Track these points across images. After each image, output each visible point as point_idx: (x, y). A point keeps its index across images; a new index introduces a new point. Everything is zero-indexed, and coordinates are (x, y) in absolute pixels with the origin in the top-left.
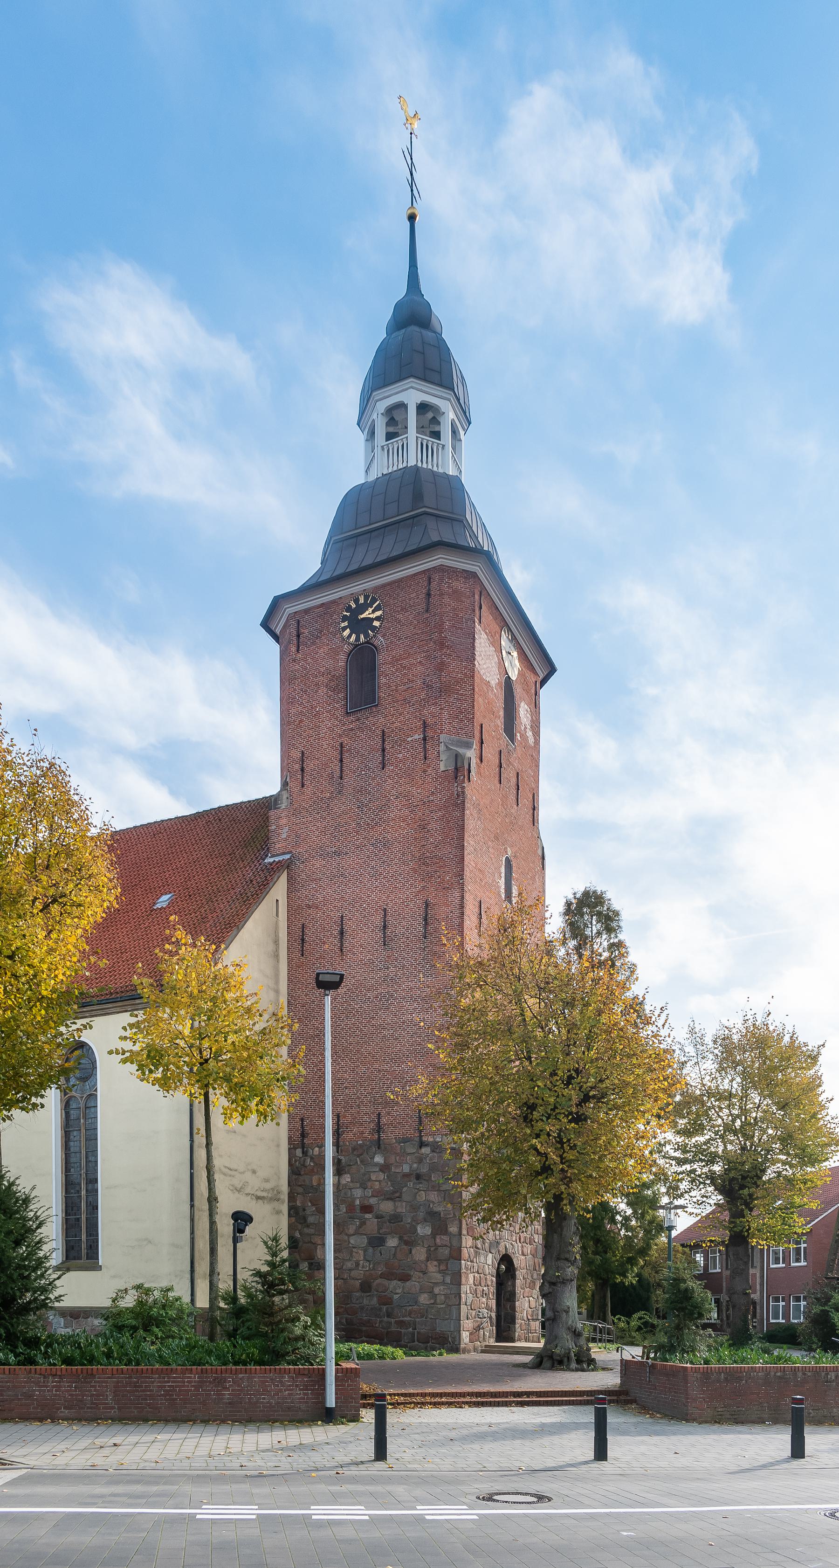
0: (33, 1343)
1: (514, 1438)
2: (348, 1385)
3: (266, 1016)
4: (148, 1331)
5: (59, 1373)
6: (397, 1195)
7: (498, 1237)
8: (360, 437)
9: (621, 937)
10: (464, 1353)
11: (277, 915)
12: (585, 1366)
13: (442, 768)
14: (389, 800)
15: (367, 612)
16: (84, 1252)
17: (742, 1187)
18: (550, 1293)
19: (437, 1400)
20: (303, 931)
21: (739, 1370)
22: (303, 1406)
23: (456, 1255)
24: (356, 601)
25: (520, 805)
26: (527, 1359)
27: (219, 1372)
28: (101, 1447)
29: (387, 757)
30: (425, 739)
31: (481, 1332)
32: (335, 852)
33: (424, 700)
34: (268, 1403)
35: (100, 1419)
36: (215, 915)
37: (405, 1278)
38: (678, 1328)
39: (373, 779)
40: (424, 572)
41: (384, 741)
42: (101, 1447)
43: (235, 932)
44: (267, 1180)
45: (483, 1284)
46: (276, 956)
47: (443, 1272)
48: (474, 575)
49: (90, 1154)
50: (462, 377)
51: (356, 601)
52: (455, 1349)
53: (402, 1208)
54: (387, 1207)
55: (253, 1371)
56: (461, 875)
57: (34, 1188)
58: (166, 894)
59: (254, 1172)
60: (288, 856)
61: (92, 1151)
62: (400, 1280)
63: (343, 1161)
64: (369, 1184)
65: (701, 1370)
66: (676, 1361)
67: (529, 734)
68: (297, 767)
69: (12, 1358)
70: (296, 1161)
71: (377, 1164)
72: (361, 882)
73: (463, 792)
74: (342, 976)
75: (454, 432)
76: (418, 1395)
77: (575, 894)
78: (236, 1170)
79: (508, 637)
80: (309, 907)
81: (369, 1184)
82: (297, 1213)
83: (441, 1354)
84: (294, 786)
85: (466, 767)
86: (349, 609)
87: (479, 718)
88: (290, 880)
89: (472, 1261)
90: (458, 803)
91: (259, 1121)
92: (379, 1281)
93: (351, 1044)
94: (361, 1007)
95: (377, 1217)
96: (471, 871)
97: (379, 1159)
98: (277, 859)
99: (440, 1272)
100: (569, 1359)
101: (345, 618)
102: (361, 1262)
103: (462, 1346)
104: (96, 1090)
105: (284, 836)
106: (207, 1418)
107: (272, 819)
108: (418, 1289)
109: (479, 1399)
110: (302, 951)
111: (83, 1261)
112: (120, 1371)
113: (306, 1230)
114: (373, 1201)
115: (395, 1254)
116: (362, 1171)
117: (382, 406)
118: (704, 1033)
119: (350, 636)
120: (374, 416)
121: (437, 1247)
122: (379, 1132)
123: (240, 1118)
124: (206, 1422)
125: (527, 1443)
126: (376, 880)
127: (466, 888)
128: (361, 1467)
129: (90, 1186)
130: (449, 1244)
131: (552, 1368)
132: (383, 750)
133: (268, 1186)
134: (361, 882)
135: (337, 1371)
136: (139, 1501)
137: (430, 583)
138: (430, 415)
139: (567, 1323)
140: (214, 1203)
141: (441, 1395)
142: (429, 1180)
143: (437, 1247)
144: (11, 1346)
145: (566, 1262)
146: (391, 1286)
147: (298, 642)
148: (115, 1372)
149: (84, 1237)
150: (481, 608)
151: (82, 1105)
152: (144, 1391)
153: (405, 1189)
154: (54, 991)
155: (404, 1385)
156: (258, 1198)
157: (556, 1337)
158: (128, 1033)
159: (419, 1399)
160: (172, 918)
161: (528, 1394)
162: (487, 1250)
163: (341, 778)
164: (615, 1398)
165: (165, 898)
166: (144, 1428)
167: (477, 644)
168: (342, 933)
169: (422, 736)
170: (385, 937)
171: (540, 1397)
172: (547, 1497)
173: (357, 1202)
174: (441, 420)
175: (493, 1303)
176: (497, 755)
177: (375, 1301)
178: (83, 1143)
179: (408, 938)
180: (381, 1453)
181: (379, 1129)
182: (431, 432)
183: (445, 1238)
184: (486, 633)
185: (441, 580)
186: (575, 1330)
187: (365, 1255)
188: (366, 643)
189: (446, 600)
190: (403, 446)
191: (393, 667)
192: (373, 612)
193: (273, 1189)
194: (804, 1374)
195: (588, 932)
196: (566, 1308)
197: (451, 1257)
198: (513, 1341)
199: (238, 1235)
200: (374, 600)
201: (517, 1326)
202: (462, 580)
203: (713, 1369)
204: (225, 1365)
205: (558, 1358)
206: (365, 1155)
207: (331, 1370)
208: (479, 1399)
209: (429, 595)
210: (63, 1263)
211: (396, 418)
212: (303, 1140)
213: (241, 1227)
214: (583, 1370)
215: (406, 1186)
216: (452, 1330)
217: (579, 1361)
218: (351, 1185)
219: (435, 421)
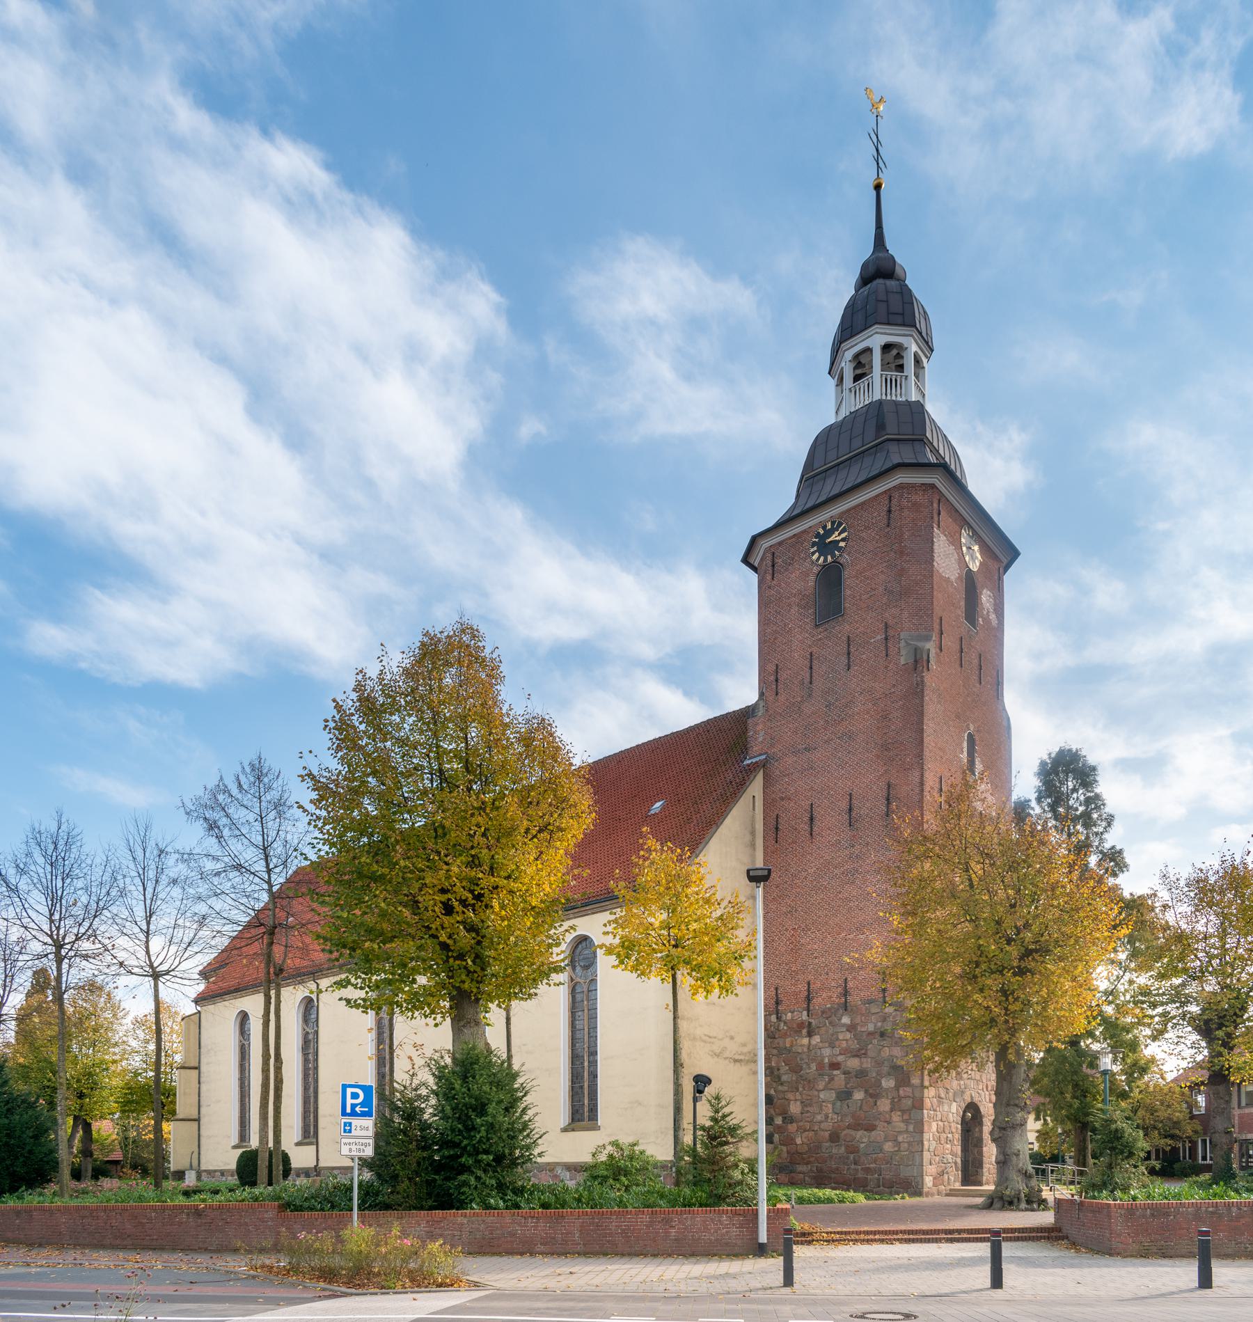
0: (519, 1191)
1: (927, 1269)
2: (779, 1223)
3: (723, 905)
4: (618, 1180)
5: (536, 1215)
6: (863, 1052)
7: (963, 1087)
8: (832, 383)
9: (1098, 790)
10: (927, 1196)
11: (754, 809)
12: (1035, 1206)
13: (903, 662)
14: (854, 696)
15: (834, 536)
16: (586, 1114)
17: (1220, 1026)
18: (1000, 1137)
19: (871, 1237)
20: (777, 820)
21: (1166, 1206)
22: (739, 1242)
23: (919, 1105)
24: (824, 527)
25: (983, 683)
26: (979, 1200)
27: (666, 1213)
28: (559, 1274)
29: (852, 658)
30: (886, 639)
31: (946, 1176)
32: (805, 749)
33: (885, 604)
34: (709, 1239)
35: (569, 1253)
36: (698, 816)
37: (870, 1128)
38: (1110, 1167)
39: (839, 680)
40: (881, 494)
41: (849, 645)
42: (559, 1274)
43: (713, 830)
44: (744, 1045)
45: (947, 1131)
46: (753, 845)
47: (906, 1122)
48: (933, 486)
49: (592, 1030)
50: (925, 312)
51: (824, 527)
52: (918, 1192)
53: (867, 1064)
54: (853, 1063)
55: (696, 1212)
56: (920, 756)
57: (523, 1065)
58: (659, 801)
59: (732, 1038)
60: (763, 757)
61: (593, 1028)
62: (865, 1130)
63: (813, 1024)
64: (837, 1043)
65: (1125, 1207)
66: (1105, 1198)
67: (993, 617)
68: (772, 678)
69: (501, 1203)
70: (771, 1026)
71: (844, 1025)
72: (829, 772)
73: (923, 681)
74: (769, 871)
75: (918, 361)
76: (853, 1232)
77: (1050, 754)
78: (715, 1038)
79: (968, 534)
80: (782, 799)
81: (837, 1043)
82: (772, 1073)
83: (903, 1198)
84: (770, 695)
85: (925, 657)
86: (818, 535)
87: (938, 611)
88: (766, 778)
89: (935, 1110)
90: (917, 692)
91: (721, 994)
92: (847, 1131)
93: (820, 917)
94: (829, 883)
95: (844, 1074)
96: (930, 751)
97: (846, 1020)
98: (754, 760)
99: (903, 1121)
100: (1019, 1199)
101: (814, 544)
102: (830, 1115)
103: (925, 1190)
104: (596, 976)
105: (761, 739)
106: (656, 1253)
107: (750, 727)
108: (883, 1138)
109: (911, 1236)
110: (776, 838)
111: (585, 1123)
112: (585, 1213)
113: (780, 1088)
114: (840, 1058)
115: (861, 1107)
116: (831, 1032)
117: (849, 355)
118: (1179, 877)
119: (818, 559)
120: (843, 364)
121: (900, 1098)
122: (845, 995)
123: (705, 993)
124: (655, 1256)
125: (935, 1274)
126: (842, 769)
127: (925, 767)
128: (769, 1292)
129: (591, 1058)
130: (911, 1095)
131: (1002, 1208)
132: (849, 654)
133: (745, 1050)
134: (829, 772)
135: (769, 1211)
136: (565, 1313)
137: (890, 501)
138: (894, 352)
139: (1017, 1166)
140: (680, 1068)
141: (875, 1233)
142: (892, 1037)
143: (900, 1098)
144: (503, 1194)
145: (1016, 1108)
146: (858, 1136)
147: (773, 571)
148: (581, 1214)
149: (586, 1102)
150: (939, 514)
151: (585, 990)
152: (604, 1230)
153: (870, 1046)
154: (542, 902)
155: (845, 1224)
156: (736, 1061)
157: (1007, 1179)
158: (609, 929)
159: (853, 1236)
160: (644, 829)
161: (959, 1231)
162: (951, 1098)
163: (811, 683)
164: (1047, 1234)
165: (658, 804)
166: (603, 1260)
167: (936, 546)
168: (812, 819)
169: (883, 636)
170: (850, 818)
171: (972, 1234)
172: (912, 1315)
173: (826, 1060)
174: (904, 354)
175: (958, 1149)
176: (958, 642)
177: (843, 1149)
178: (586, 1022)
179: (871, 818)
180: (788, 1280)
181: (846, 993)
182: (896, 366)
183: (907, 1089)
184: (945, 535)
185: (901, 496)
186: (1026, 1172)
187: (833, 1108)
188: (833, 562)
189: (906, 513)
190: (868, 384)
191: (857, 579)
192: (839, 534)
193: (750, 1052)
194: (1240, 1209)
195: (1064, 789)
196: (1016, 1151)
197: (914, 1107)
198: (980, 1184)
199: (697, 1095)
200: (840, 524)
201: (985, 1170)
202: (921, 493)
203: (1138, 1205)
204: (673, 1207)
205: (1009, 1199)
206: (833, 1017)
207: (763, 1210)
208: (911, 1236)
209: (889, 511)
210: (569, 1124)
211: (863, 362)
212: (777, 1007)
213: (701, 1088)
214: (1033, 1210)
215: (871, 1043)
216: (915, 1175)
217: (1029, 1202)
218: (821, 1044)
219: (899, 356)
